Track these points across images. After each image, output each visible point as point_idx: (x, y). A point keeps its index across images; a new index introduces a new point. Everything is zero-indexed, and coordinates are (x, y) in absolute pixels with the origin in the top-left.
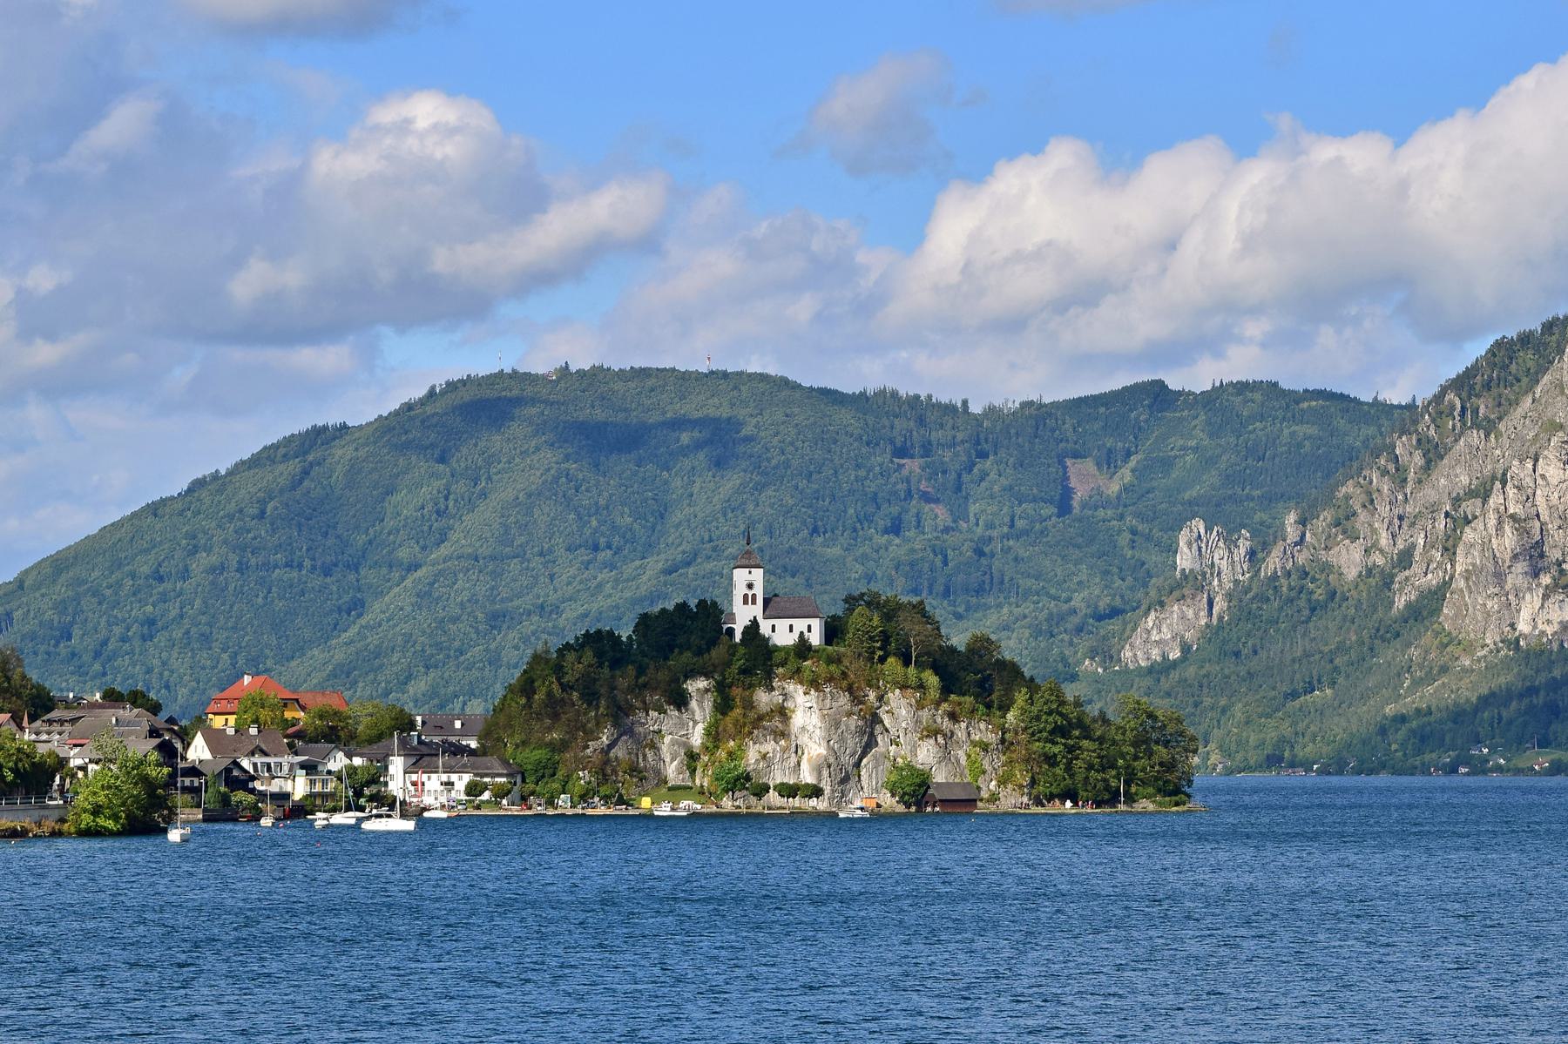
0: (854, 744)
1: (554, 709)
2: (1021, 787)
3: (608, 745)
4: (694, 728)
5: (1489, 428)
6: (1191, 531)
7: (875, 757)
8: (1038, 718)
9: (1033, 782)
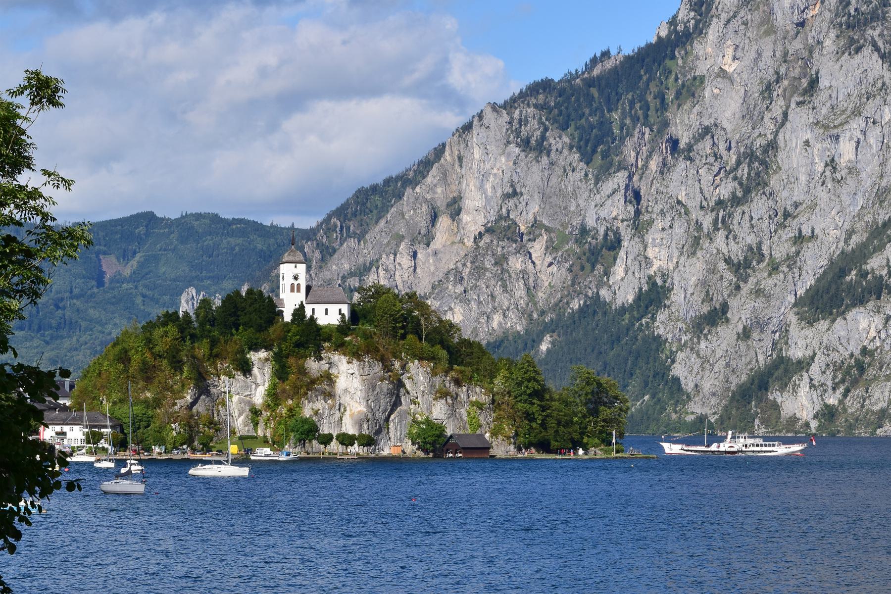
0: (384, 402)
1: (148, 373)
2: (509, 438)
3: (191, 403)
4: (256, 389)
5: (360, 237)
6: (188, 294)
7: (400, 415)
8: (520, 384)
9: (517, 434)
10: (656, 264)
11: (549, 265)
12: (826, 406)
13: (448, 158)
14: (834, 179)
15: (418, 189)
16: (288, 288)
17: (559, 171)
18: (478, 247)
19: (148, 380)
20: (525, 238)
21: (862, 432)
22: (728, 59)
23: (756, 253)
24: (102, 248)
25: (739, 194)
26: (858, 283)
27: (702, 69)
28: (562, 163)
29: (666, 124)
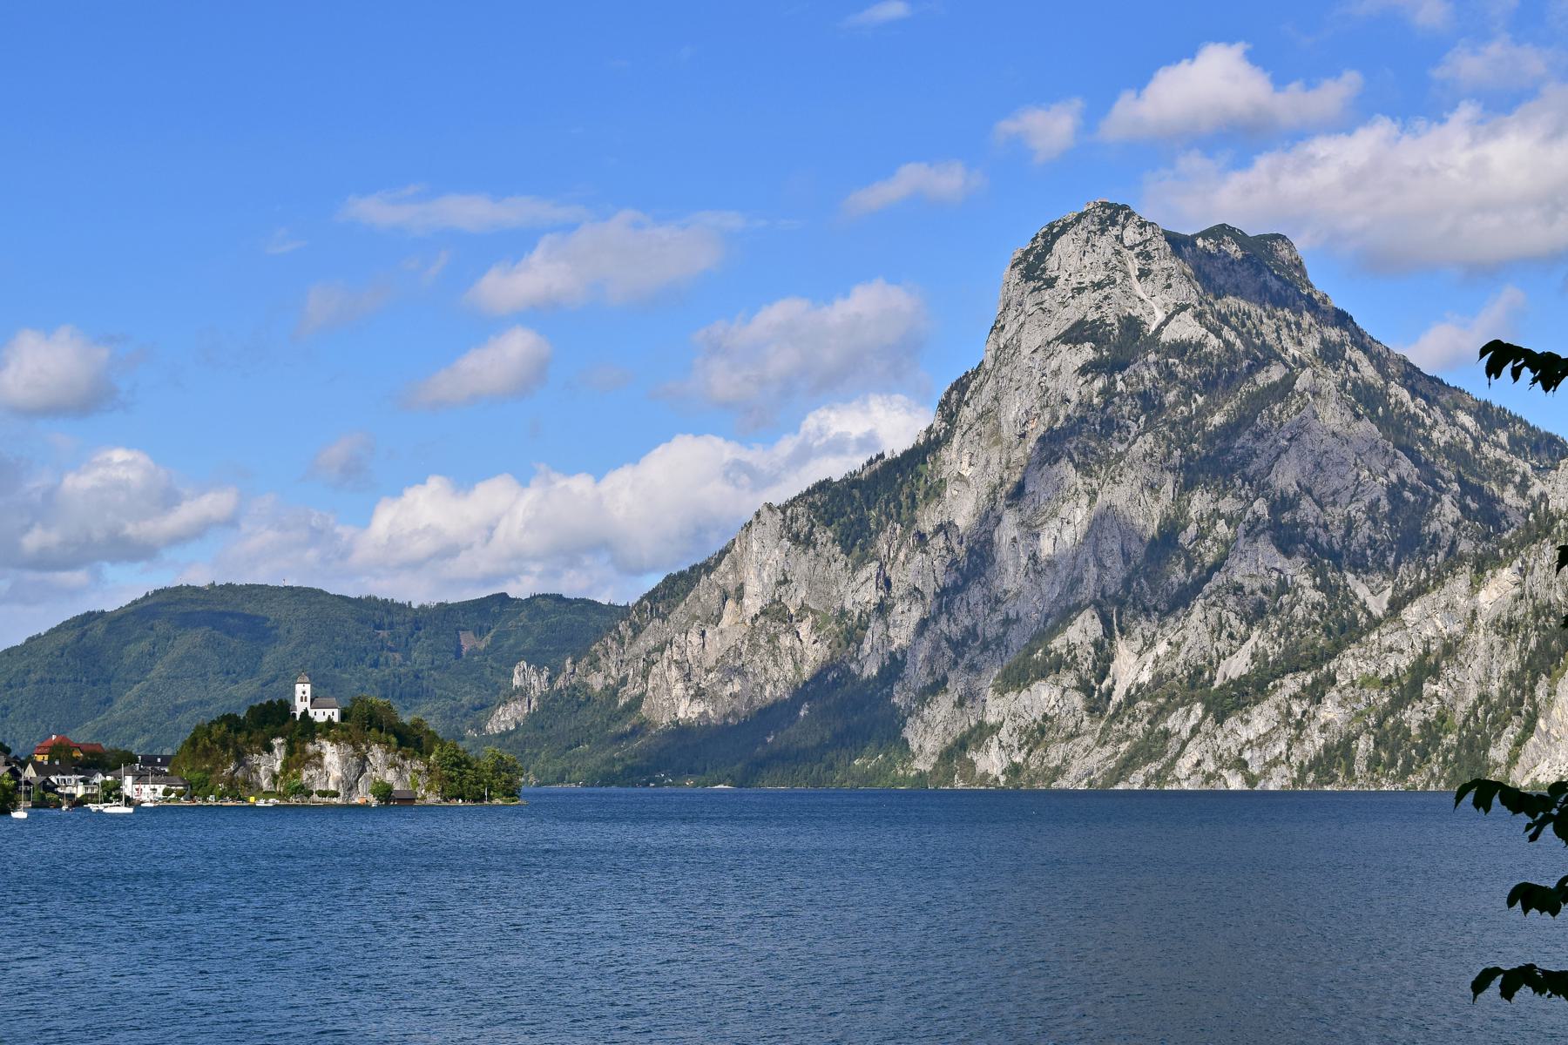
1: (207, 752)
5: (664, 618)
9: (443, 790)
10: (897, 642)
11: (815, 642)
12: (1013, 763)
13: (738, 549)
14: (1035, 571)
15: (712, 576)
17: (824, 562)
18: (754, 627)
19: (207, 756)
20: (794, 619)
21: (1040, 785)
22: (965, 465)
23: (971, 633)
24: (462, 625)
25: (960, 583)
26: (1043, 660)
27: (945, 472)
28: (826, 554)
29: (914, 521)
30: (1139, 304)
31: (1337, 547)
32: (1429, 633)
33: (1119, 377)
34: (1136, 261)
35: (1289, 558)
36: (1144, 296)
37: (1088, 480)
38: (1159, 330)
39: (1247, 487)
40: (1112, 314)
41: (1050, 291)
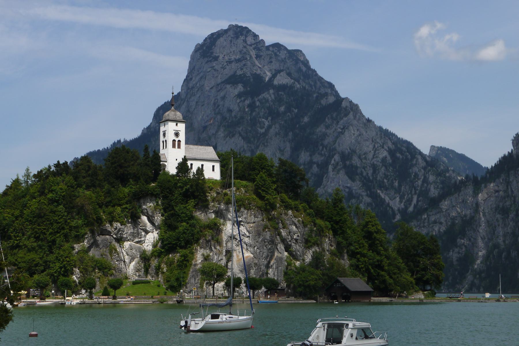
4: (145, 236)
16: (170, 144)
30: (259, 69)
31: (371, 178)
32: (454, 214)
33: (256, 99)
34: (253, 51)
35: (354, 182)
36: (260, 66)
37: (249, 145)
38: (271, 80)
39: (325, 150)
40: (249, 72)
41: (216, 62)
